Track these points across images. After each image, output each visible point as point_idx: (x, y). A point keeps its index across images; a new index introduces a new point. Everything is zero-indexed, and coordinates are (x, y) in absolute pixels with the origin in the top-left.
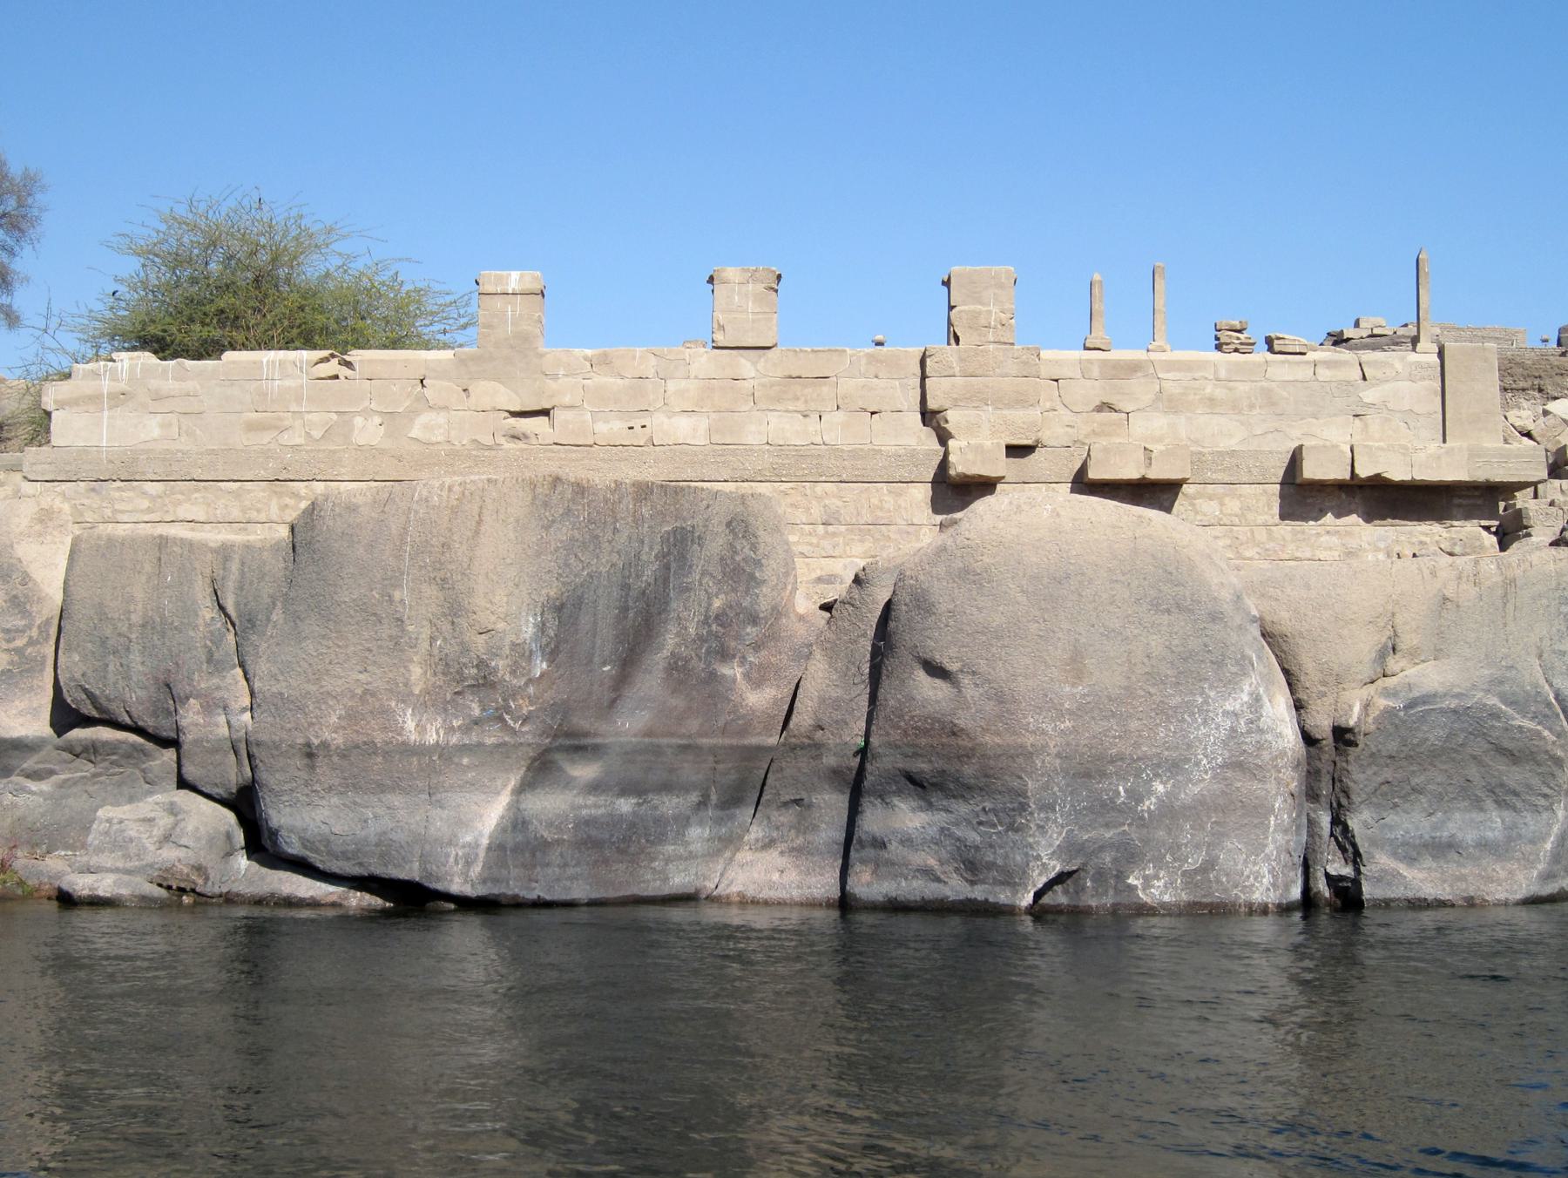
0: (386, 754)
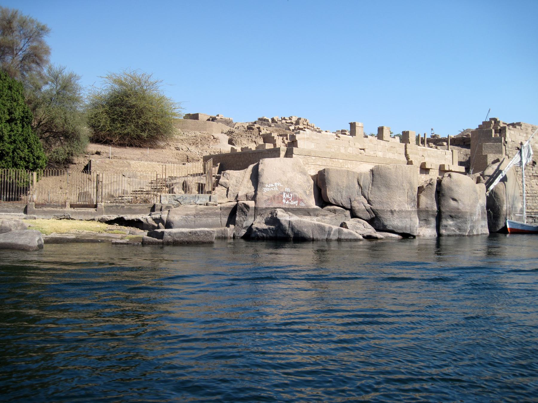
0: (405, 212)
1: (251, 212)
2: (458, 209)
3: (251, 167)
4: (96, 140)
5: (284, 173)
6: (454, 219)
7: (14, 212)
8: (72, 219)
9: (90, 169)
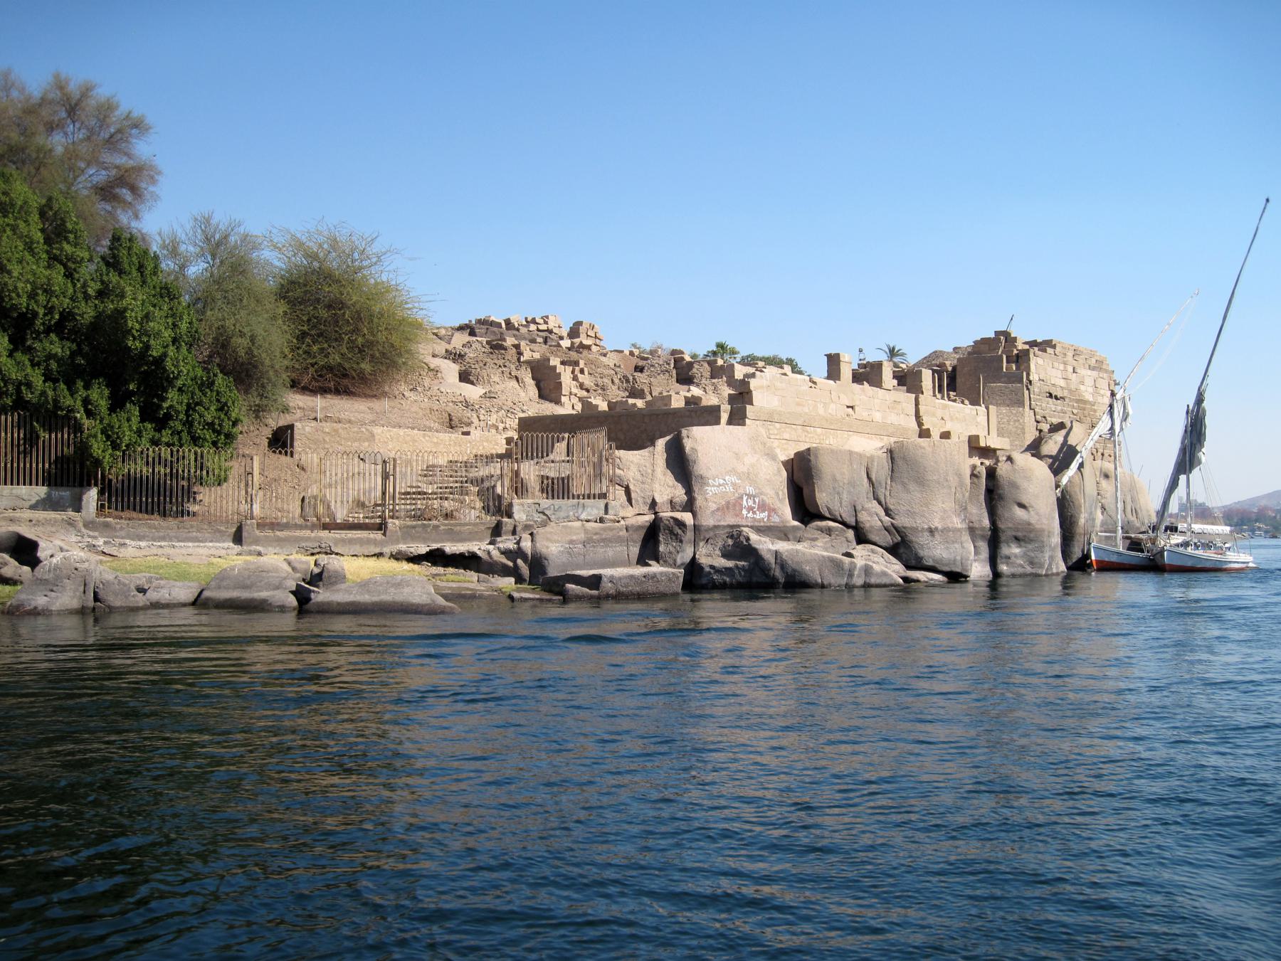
1: (690, 535)
2: (1029, 524)
3: (661, 443)
4: (294, 385)
5: (737, 456)
6: (1022, 543)
7: (211, 541)
8: (337, 554)
9: (292, 446)
